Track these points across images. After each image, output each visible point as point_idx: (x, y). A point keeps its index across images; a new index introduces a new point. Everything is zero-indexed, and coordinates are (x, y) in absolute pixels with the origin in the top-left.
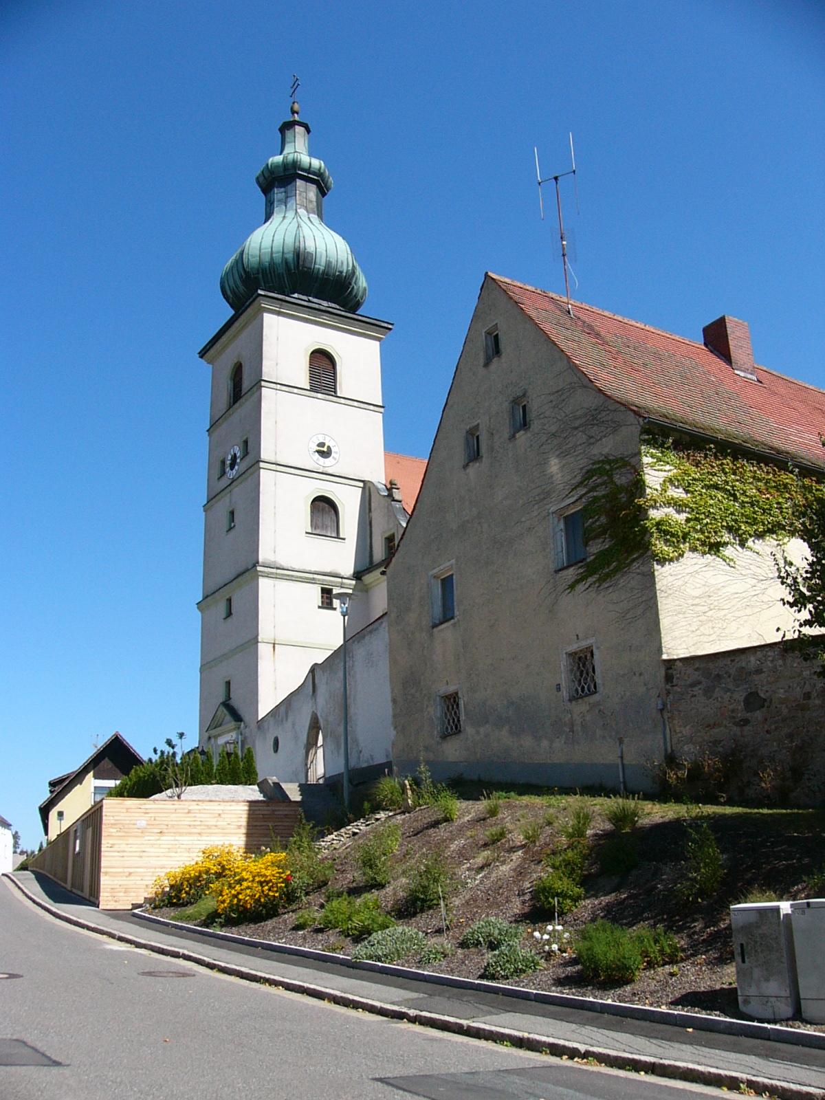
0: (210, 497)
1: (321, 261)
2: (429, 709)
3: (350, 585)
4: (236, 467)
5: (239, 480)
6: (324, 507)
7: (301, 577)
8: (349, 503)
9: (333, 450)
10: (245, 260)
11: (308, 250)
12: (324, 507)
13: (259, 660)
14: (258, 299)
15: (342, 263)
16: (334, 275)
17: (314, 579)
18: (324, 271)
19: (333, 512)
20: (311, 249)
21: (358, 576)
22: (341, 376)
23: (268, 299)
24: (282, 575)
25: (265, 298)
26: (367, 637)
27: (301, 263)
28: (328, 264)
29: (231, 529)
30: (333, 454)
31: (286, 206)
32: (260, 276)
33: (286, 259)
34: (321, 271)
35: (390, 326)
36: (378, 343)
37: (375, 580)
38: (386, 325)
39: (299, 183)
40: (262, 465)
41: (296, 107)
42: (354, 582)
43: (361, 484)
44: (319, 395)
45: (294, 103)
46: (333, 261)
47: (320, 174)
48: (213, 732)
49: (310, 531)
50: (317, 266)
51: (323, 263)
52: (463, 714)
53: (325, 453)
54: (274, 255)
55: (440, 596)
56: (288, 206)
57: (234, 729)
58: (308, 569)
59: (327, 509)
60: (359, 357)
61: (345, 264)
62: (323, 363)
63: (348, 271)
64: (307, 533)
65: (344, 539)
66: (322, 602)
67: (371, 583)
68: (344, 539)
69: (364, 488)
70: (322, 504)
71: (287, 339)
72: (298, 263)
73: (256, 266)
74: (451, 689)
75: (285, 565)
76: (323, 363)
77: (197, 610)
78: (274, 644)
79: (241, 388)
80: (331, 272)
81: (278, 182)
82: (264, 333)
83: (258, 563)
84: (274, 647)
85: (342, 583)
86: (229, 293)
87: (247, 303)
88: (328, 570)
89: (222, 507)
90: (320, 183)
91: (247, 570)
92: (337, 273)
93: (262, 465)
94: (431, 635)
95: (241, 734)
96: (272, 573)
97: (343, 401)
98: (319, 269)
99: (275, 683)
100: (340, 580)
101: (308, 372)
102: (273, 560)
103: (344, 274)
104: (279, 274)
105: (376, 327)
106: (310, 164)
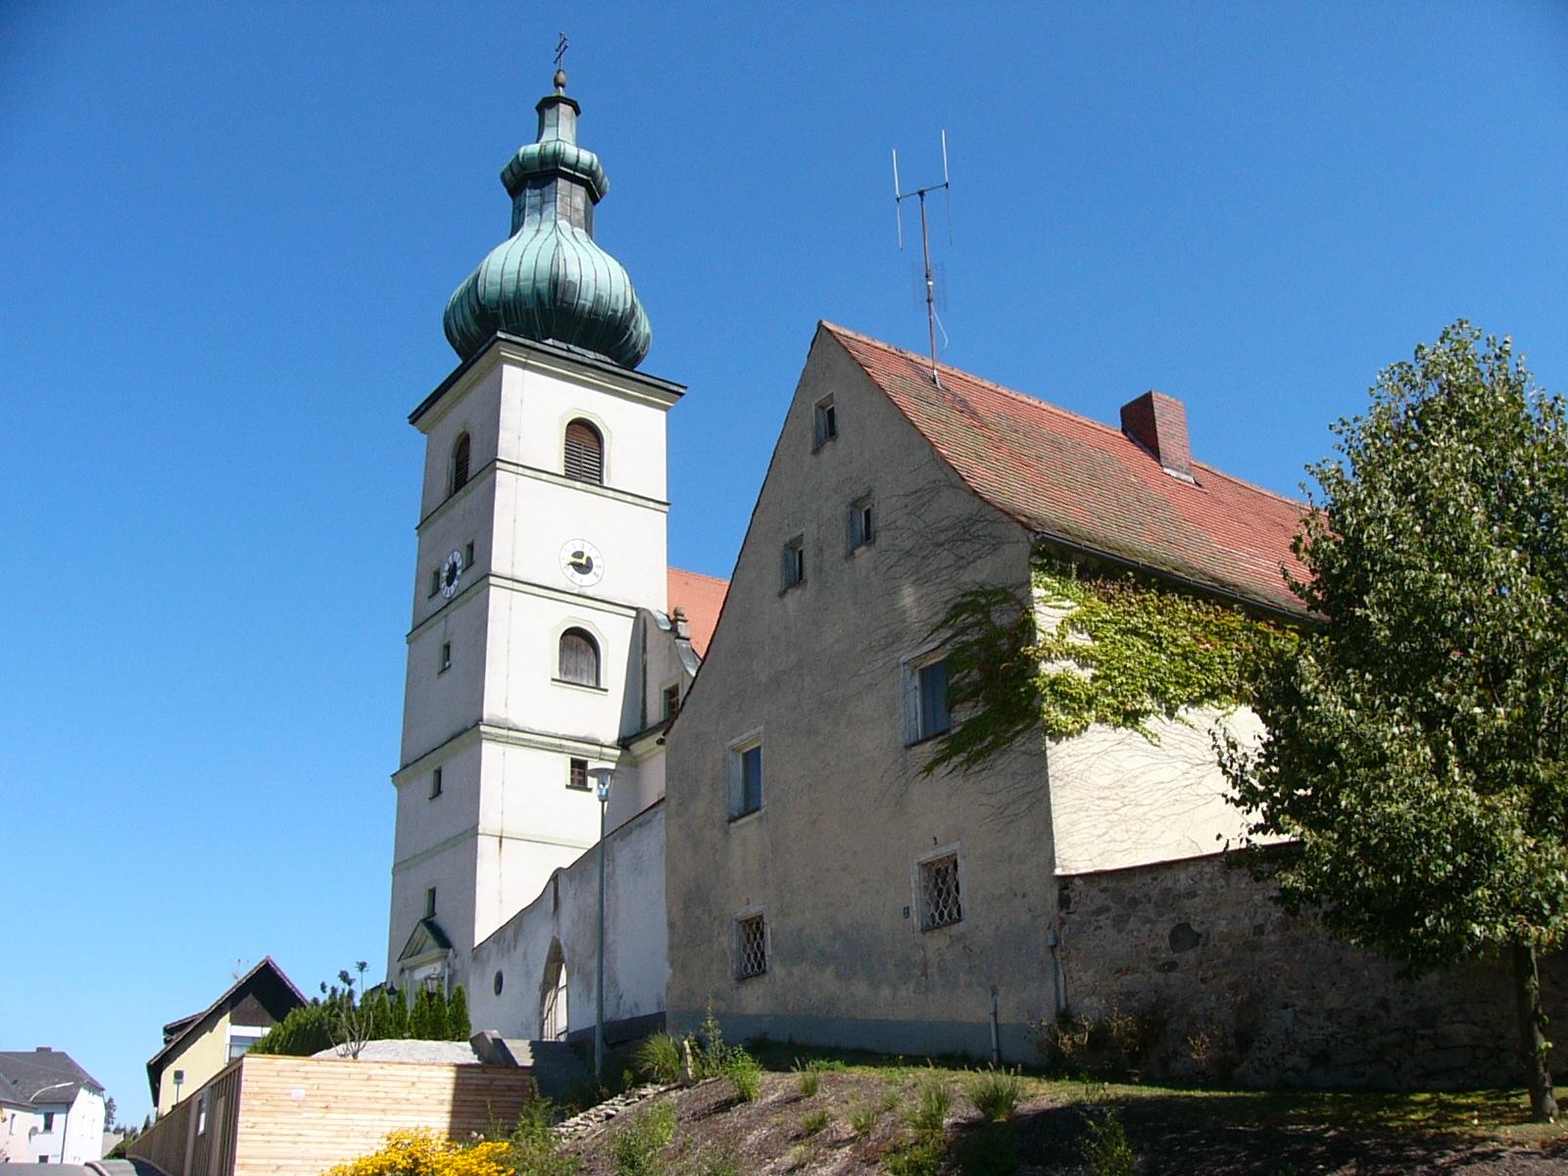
3: (613, 756)
4: (456, 582)
6: (579, 644)
7: (542, 743)
8: (615, 640)
10: (480, 289)
11: (570, 278)
12: (579, 644)
15: (617, 298)
16: (605, 316)
17: (561, 746)
21: (624, 743)
27: (559, 295)
28: (598, 299)
29: (444, 670)
30: (594, 569)
31: (541, 215)
32: (501, 310)
34: (587, 308)
35: (682, 391)
36: (663, 414)
37: (647, 752)
38: (675, 388)
39: (561, 183)
41: (562, 77)
42: (618, 753)
43: (633, 613)
44: (578, 485)
46: (605, 295)
47: (590, 172)
49: (558, 678)
50: (582, 302)
51: (591, 297)
53: (583, 567)
60: (636, 433)
62: (584, 438)
64: (553, 680)
65: (606, 690)
68: (606, 690)
69: (636, 619)
70: (577, 640)
71: (534, 403)
75: (521, 726)
78: (501, 837)
79: (467, 469)
81: (532, 179)
83: (482, 720)
84: (501, 842)
85: (601, 753)
88: (581, 734)
89: (434, 637)
92: (610, 313)
94: (727, 832)
96: (502, 736)
97: (611, 493)
98: (584, 305)
99: (500, 893)
100: (598, 748)
101: (563, 451)
102: (504, 717)
103: (620, 314)
105: (662, 391)
106: (578, 157)
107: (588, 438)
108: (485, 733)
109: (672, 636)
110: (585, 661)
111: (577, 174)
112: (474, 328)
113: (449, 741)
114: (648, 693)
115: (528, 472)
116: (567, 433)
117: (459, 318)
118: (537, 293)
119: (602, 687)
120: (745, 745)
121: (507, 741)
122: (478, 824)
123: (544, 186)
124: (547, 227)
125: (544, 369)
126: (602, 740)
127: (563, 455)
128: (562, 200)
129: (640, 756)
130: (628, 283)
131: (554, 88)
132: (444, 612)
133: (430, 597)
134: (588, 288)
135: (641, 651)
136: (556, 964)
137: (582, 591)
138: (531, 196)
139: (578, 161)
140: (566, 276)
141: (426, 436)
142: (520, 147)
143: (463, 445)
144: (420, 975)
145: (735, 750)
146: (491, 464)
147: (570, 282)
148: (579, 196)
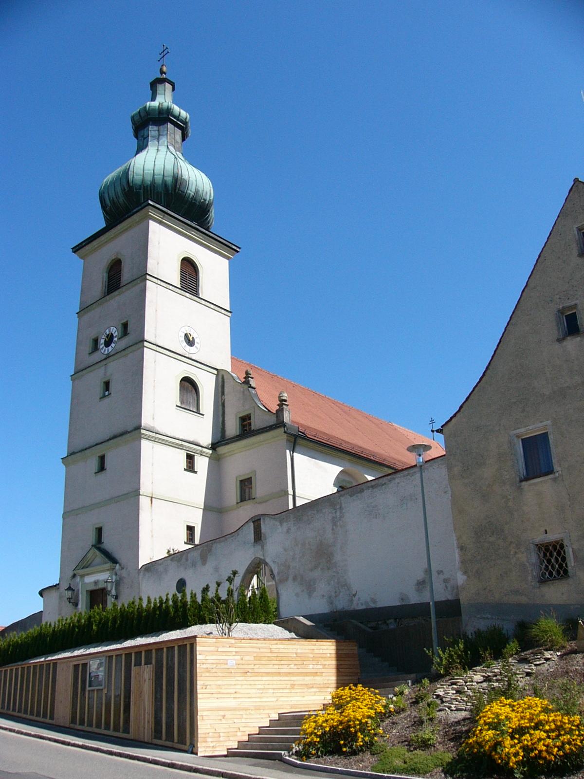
0: (82, 367)
1: (192, 188)
2: (519, 555)
3: (208, 453)
4: (113, 345)
5: (115, 357)
6: (188, 385)
7: (173, 443)
8: (207, 385)
9: (196, 340)
10: (130, 177)
11: (184, 177)
12: (188, 385)
13: (140, 511)
14: (147, 207)
15: (206, 193)
16: (200, 202)
17: (182, 445)
18: (192, 198)
19: (194, 391)
20: (185, 177)
21: (214, 446)
22: (202, 282)
23: (154, 209)
24: (160, 439)
25: (152, 208)
26: (365, 491)
27: (178, 186)
28: (197, 191)
29: (104, 396)
30: (196, 344)
31: (158, 142)
32: (142, 191)
33: (166, 181)
34: (191, 196)
35: (238, 250)
36: (227, 261)
37: (228, 452)
38: (235, 248)
39: (170, 125)
40: (146, 344)
41: (165, 69)
42: (210, 452)
43: (215, 372)
44: (188, 295)
45: (163, 65)
46: (200, 189)
47: (185, 123)
48: (81, 572)
49: (179, 405)
50: (189, 192)
51: (193, 190)
52: (572, 561)
53: (190, 342)
54: (155, 177)
55: (522, 454)
56: (160, 142)
57: (108, 570)
58: (177, 436)
59: (190, 388)
60: (215, 269)
61: (208, 194)
62: (189, 267)
63: (210, 200)
64: (177, 406)
65: (203, 415)
66: (187, 466)
67: (224, 454)
68: (203, 415)
69: (217, 375)
70: (187, 384)
71: (166, 245)
72: (176, 186)
73: (139, 183)
74: (552, 537)
75: (161, 431)
76: (189, 267)
77: (62, 464)
78: (152, 497)
79: (121, 280)
80: (198, 199)
81: (147, 124)
82: (149, 236)
83: (140, 426)
84: (151, 500)
85: (202, 451)
86: (108, 202)
87: (135, 210)
88: (191, 439)
89: (95, 378)
90: (183, 127)
91: (125, 433)
92: (202, 200)
93: (146, 344)
94: (519, 488)
95: (116, 574)
96: (152, 437)
97: (203, 302)
98: (190, 194)
99: (152, 531)
100: (200, 448)
101: (180, 275)
102: (152, 425)
103: (207, 202)
104: (158, 192)
105: (225, 246)
106: (180, 113)
107: (190, 269)
108: (143, 434)
109: (246, 386)
110: (191, 398)
111: (178, 122)
112: (122, 200)
113: (108, 440)
114: (226, 418)
115: (163, 284)
116: (181, 265)
117: (112, 193)
118: (165, 183)
119: (201, 413)
120: (523, 436)
121: (155, 440)
122: (140, 489)
123: (160, 126)
124: (163, 149)
125: (171, 226)
126: (202, 444)
127: (179, 278)
128: (170, 135)
129: (221, 455)
130: (211, 186)
131: (159, 73)
132: (105, 362)
133: (90, 354)
134: (192, 185)
135: (220, 394)
136: (251, 575)
137: (190, 356)
138: (152, 130)
139: (179, 115)
140: (182, 176)
141: (82, 261)
142: (147, 102)
143: (115, 269)
144: (90, 579)
145: (518, 437)
146: (142, 276)
147: (184, 179)
148: (178, 133)
